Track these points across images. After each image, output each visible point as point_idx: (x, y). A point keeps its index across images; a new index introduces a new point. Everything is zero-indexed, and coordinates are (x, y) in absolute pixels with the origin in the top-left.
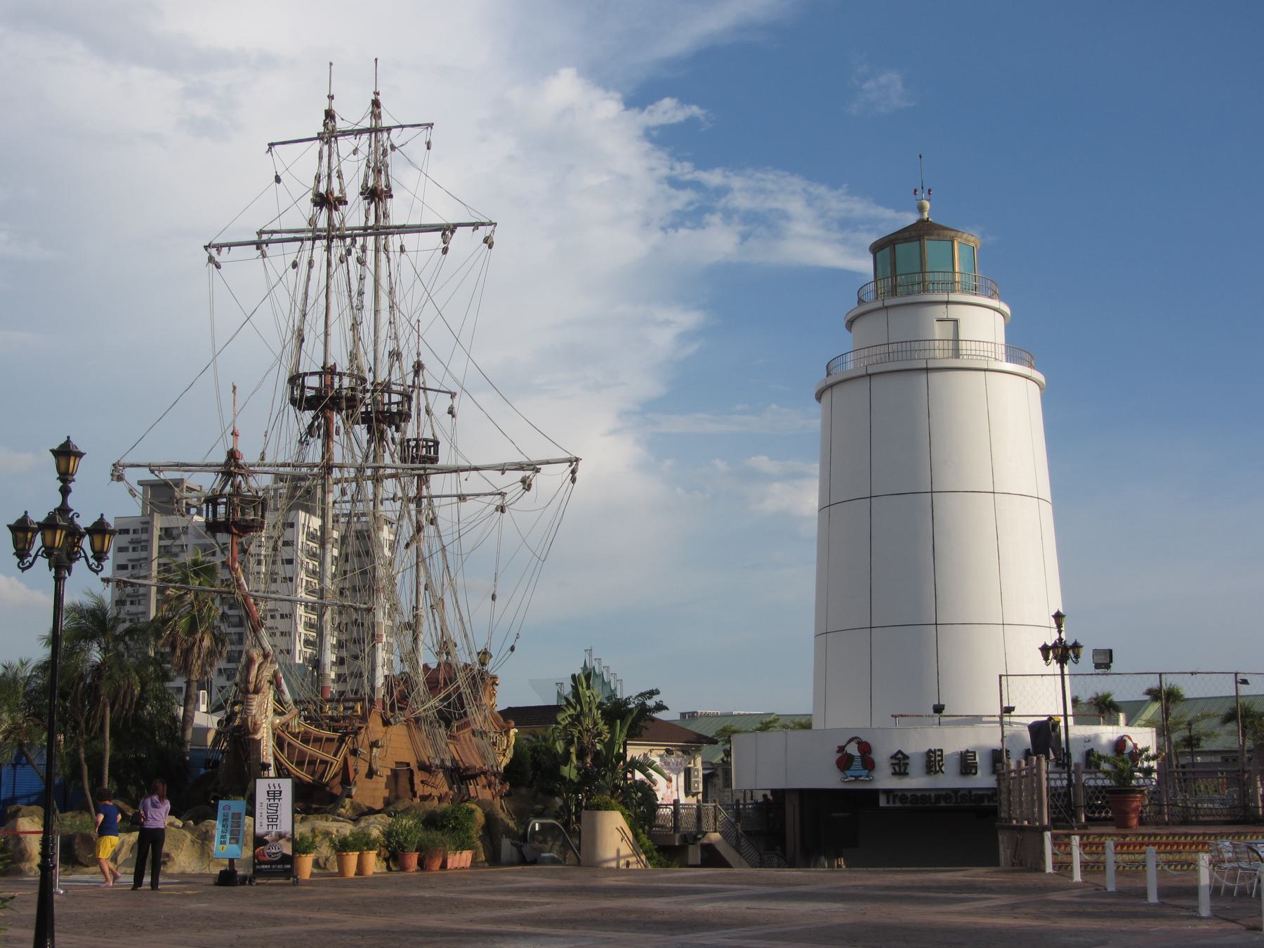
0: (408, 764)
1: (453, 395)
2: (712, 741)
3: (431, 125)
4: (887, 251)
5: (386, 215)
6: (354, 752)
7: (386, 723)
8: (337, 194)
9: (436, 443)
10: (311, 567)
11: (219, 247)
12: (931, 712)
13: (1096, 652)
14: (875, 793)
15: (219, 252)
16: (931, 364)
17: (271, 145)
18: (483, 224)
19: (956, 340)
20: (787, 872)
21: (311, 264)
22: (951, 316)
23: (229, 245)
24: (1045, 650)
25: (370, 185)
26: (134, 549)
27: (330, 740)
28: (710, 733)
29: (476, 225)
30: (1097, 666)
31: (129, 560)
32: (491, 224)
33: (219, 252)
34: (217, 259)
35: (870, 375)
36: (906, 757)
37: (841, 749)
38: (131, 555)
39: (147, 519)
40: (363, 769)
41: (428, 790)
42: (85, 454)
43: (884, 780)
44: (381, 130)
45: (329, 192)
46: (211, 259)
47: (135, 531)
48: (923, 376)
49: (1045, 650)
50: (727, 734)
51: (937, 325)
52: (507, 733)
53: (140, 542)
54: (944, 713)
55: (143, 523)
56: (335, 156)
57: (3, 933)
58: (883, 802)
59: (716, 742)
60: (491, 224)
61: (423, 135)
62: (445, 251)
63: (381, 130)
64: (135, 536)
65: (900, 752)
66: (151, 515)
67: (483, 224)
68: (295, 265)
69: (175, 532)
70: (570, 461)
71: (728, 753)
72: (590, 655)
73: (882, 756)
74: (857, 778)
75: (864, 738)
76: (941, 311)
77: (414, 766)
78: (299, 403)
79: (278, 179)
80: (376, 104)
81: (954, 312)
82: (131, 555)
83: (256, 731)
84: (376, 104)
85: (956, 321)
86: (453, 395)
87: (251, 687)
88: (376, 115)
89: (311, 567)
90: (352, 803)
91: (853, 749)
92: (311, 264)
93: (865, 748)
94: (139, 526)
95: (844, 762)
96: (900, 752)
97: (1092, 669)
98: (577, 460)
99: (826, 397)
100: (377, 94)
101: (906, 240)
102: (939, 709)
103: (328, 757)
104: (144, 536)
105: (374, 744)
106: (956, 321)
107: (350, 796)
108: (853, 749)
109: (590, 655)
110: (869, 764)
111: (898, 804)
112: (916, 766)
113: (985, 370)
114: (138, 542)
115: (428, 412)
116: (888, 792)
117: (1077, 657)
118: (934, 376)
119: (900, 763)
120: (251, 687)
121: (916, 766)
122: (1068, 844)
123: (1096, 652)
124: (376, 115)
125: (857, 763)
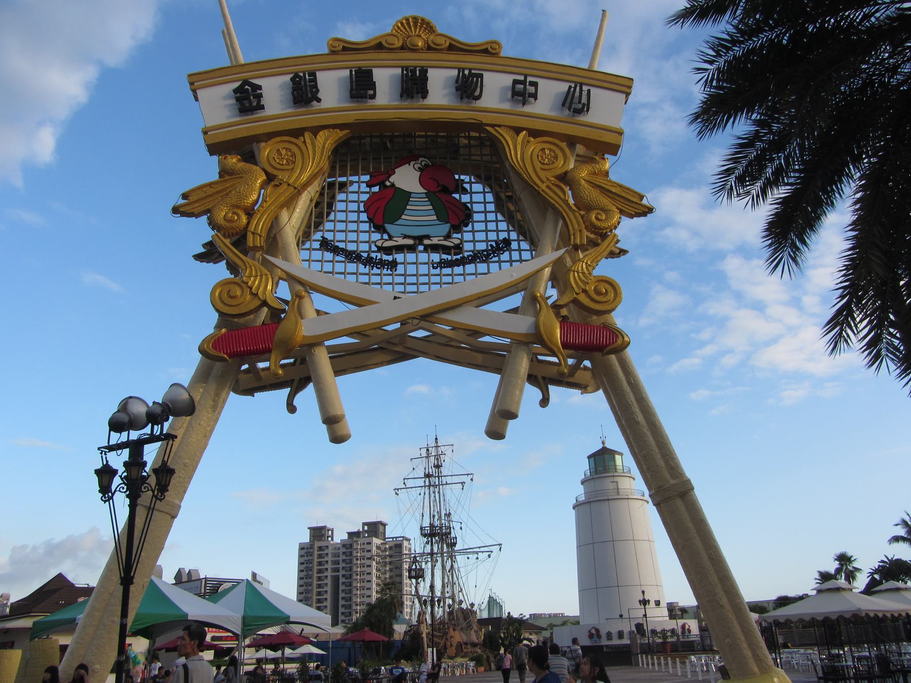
0: (460, 642)
1: (461, 523)
2: (546, 629)
3: (453, 445)
4: (592, 458)
5: (441, 472)
6: (447, 639)
7: (454, 630)
8: (431, 473)
9: (456, 538)
10: (378, 560)
11: (398, 489)
12: (619, 617)
13: (655, 601)
14: (602, 647)
15: (398, 491)
16: (610, 498)
17: (411, 459)
18: (470, 474)
19: (618, 489)
20: (288, 194)
21: (425, 494)
22: (616, 480)
23: (401, 489)
24: (640, 601)
25: (436, 464)
26: (307, 556)
27: (440, 636)
28: (545, 626)
29: (468, 475)
30: (656, 605)
31: (305, 561)
32: (472, 474)
33: (398, 491)
34: (398, 493)
35: (590, 502)
36: (611, 633)
37: (590, 631)
38: (306, 558)
39: (312, 543)
40: (449, 644)
41: (466, 650)
42: (309, 528)
43: (604, 642)
44: (438, 446)
45: (429, 473)
46: (396, 493)
47: (307, 548)
48: (607, 503)
49: (640, 601)
50: (552, 626)
51: (610, 483)
52: (481, 630)
53: (309, 553)
54: (623, 617)
55: (311, 545)
56: (430, 462)
57: (424, 677)
58: (605, 650)
59: (547, 630)
60: (472, 474)
61: (451, 448)
62: (463, 489)
63: (438, 446)
64: (307, 550)
65: (609, 632)
66: (314, 541)
67: (470, 474)
68: (420, 494)
69: (323, 548)
70: (462, 483)
71: (552, 634)
72: (491, 592)
73: (603, 632)
74: (595, 641)
75: (597, 627)
76: (612, 479)
77: (462, 643)
78: (425, 535)
79: (414, 469)
80: (436, 439)
81: (616, 479)
82: (306, 558)
83: (422, 634)
84: (436, 439)
85: (617, 482)
86: (461, 523)
87: (421, 622)
88: (437, 442)
89: (378, 560)
90: (447, 655)
91: (593, 631)
92: (425, 494)
93: (597, 631)
94: (309, 546)
95: (591, 636)
96: (609, 632)
97: (654, 606)
98: (501, 544)
99: (576, 508)
100: (436, 436)
101: (599, 455)
102: (621, 616)
103: (440, 641)
104: (311, 550)
105: (452, 637)
106: (617, 482)
107: (446, 652)
108: (593, 631)
109: (491, 592)
110: (599, 636)
111: (610, 650)
112: (615, 636)
113: (628, 499)
114: (308, 553)
115: (453, 528)
116: (607, 646)
117: (649, 604)
118: (611, 502)
119: (609, 636)
120: (421, 622)
121: (615, 636)
122: (667, 660)
123: (655, 601)
124: (437, 442)
125: (595, 636)
